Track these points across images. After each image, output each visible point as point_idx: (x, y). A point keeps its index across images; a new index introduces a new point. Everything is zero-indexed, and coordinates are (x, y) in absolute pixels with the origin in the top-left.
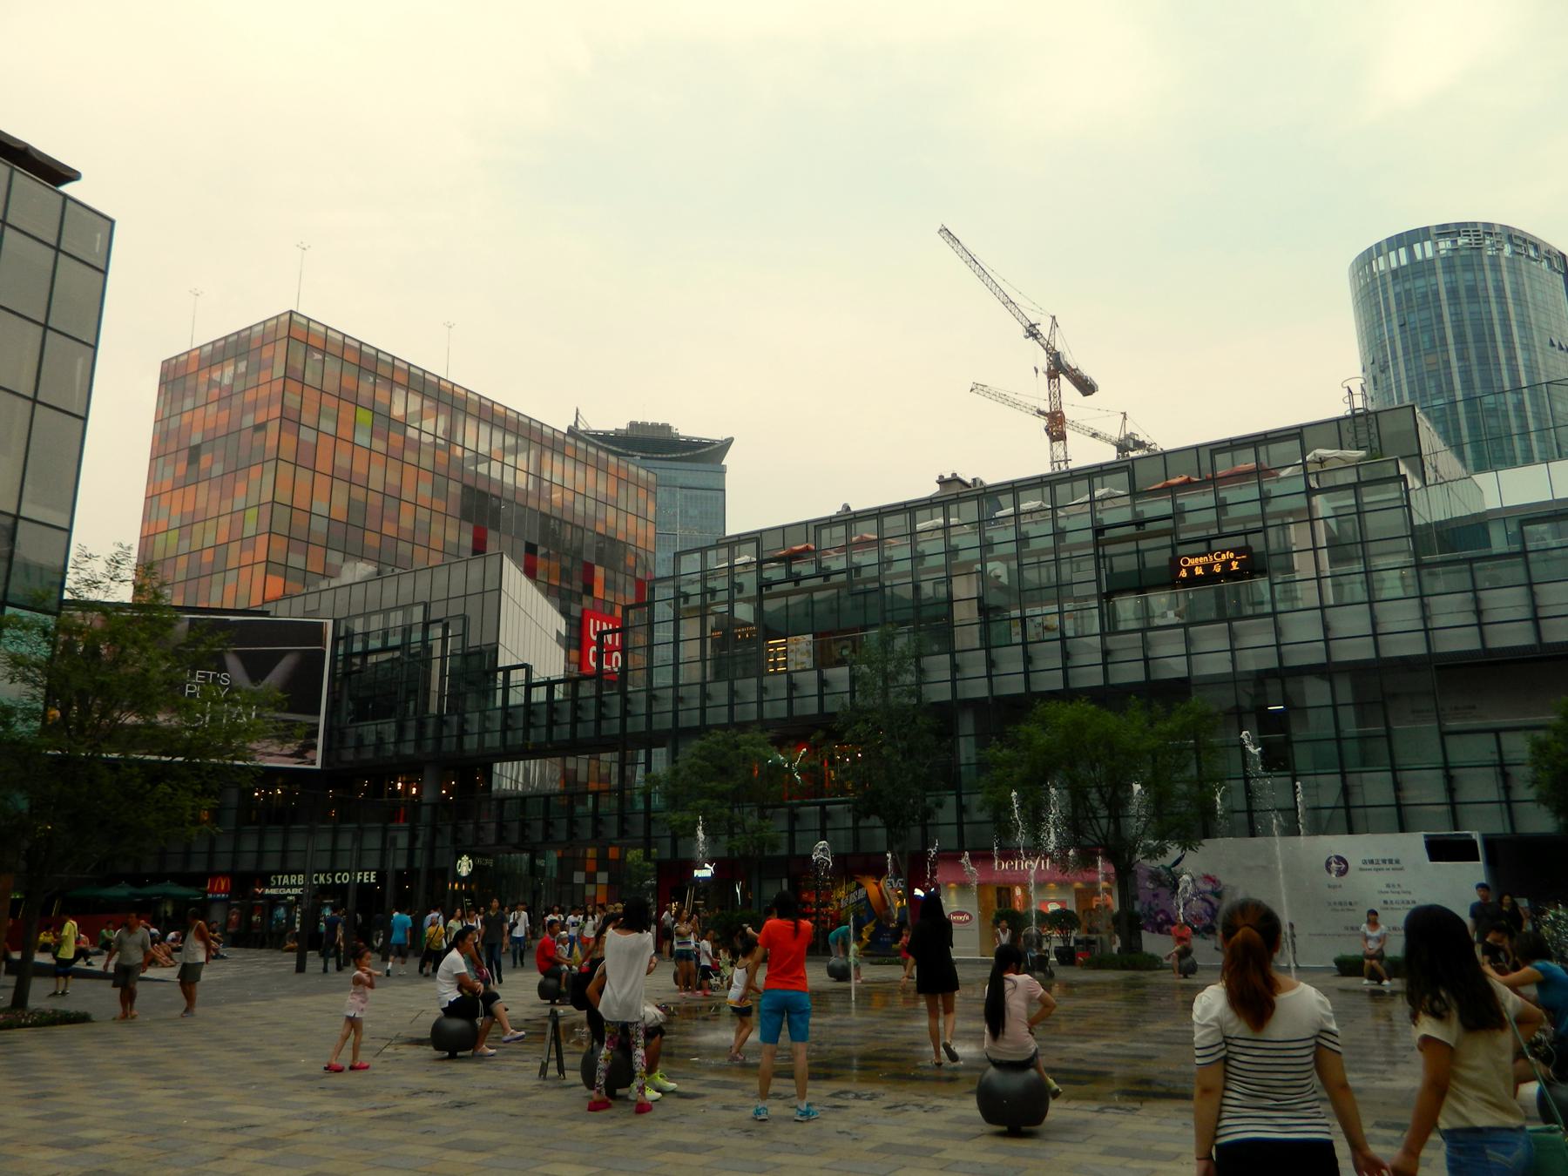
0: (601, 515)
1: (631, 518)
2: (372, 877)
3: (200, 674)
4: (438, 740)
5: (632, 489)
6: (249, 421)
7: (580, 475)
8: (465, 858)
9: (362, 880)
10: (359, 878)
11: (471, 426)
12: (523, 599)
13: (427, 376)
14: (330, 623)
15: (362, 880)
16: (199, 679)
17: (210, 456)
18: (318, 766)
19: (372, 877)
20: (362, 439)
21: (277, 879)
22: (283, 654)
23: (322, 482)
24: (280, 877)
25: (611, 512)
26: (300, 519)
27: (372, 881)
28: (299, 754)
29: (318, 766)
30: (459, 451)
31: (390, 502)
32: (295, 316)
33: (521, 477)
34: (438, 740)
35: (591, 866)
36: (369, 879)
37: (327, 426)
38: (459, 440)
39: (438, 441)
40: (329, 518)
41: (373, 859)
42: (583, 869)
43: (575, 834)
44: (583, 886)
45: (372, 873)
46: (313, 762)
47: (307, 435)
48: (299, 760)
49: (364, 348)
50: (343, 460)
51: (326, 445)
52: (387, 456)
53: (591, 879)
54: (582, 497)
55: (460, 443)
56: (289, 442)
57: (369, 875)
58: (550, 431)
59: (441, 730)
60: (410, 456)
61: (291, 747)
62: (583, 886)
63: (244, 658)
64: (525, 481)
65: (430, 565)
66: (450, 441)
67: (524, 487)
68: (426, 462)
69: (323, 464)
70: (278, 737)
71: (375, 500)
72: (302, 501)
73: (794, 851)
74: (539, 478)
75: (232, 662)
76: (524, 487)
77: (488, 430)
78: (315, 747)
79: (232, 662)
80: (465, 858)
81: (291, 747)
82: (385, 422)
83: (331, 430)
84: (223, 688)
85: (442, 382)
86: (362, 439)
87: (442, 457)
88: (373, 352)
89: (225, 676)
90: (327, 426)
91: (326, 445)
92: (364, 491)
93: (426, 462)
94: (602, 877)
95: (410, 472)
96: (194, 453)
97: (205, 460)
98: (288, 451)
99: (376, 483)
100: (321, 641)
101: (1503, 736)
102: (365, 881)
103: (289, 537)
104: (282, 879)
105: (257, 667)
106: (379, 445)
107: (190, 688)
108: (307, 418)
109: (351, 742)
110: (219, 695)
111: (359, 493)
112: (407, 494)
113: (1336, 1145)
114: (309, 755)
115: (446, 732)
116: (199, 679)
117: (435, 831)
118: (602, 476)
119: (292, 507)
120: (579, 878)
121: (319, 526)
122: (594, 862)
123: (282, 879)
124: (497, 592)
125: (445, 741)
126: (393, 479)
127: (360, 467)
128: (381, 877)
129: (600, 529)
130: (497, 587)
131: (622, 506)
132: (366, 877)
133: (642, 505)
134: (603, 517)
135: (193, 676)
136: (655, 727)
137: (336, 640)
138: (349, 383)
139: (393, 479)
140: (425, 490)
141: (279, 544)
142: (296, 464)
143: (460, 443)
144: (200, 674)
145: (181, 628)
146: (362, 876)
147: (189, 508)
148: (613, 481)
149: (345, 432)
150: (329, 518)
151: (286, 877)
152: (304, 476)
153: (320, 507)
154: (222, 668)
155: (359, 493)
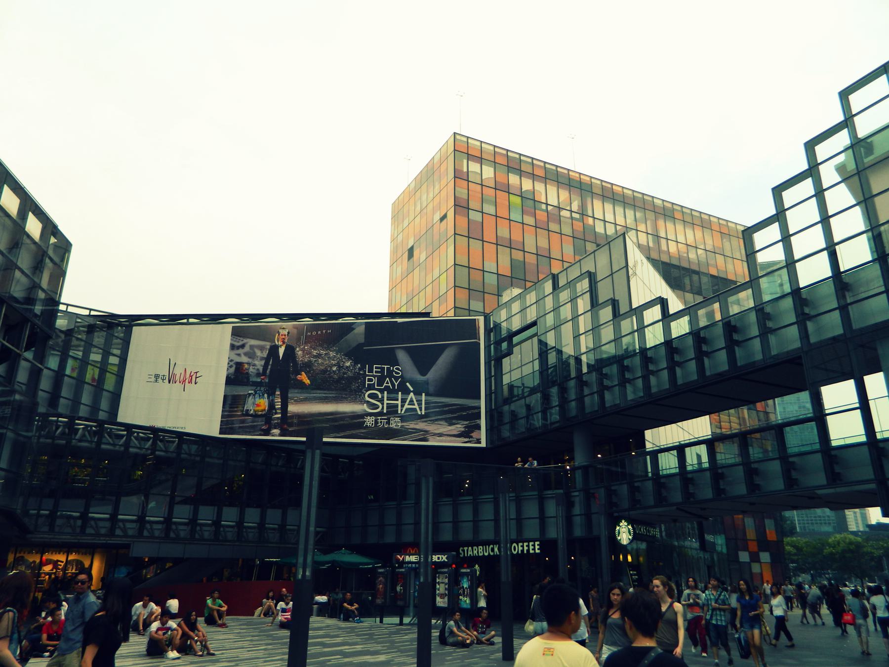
0: (711, 262)
2: (537, 547)
3: (376, 368)
4: (580, 399)
6: (437, 217)
8: (623, 523)
9: (528, 550)
10: (526, 548)
11: (597, 204)
13: (559, 169)
14: (481, 319)
15: (528, 550)
16: (376, 372)
17: (418, 250)
18: (483, 444)
19: (537, 547)
20: (516, 216)
21: (463, 551)
22: (443, 348)
23: (490, 249)
24: (466, 549)
25: (720, 259)
26: (476, 276)
27: (537, 551)
28: (465, 434)
29: (483, 444)
30: (590, 221)
31: (544, 261)
32: (458, 137)
34: (580, 399)
35: (753, 546)
36: (534, 549)
37: (489, 209)
38: (590, 213)
39: (574, 215)
40: (498, 274)
41: (532, 528)
42: (746, 549)
43: (758, 487)
44: (749, 564)
45: (537, 543)
46: (479, 441)
48: (466, 440)
49: (510, 154)
50: (504, 232)
51: (489, 223)
52: (536, 227)
53: (755, 558)
54: (602, 223)
56: (463, 222)
57: (534, 545)
58: (660, 202)
59: (582, 390)
60: (553, 226)
61: (459, 427)
62: (749, 564)
63: (410, 351)
65: (565, 267)
66: (583, 214)
67: (646, 244)
68: (567, 230)
69: (489, 236)
70: (446, 420)
71: (531, 259)
72: (476, 263)
73: (380, 619)
74: (657, 237)
75: (402, 356)
76: (646, 244)
78: (478, 427)
79: (402, 356)
80: (623, 523)
81: (459, 427)
82: (530, 202)
83: (493, 212)
84: (396, 379)
85: (571, 173)
86: (516, 216)
87: (578, 226)
88: (517, 156)
89: (397, 369)
90: (489, 209)
92: (522, 253)
93: (567, 230)
94: (765, 557)
95: (555, 238)
96: (411, 252)
97: (416, 253)
98: (463, 229)
99: (530, 246)
100: (476, 335)
102: (531, 551)
103: (469, 289)
104: (467, 550)
105: (423, 361)
106: (529, 220)
107: (370, 380)
109: (507, 419)
110: (393, 385)
111: (518, 256)
112: (555, 254)
114: (474, 435)
115: (586, 391)
116: (376, 372)
117: (589, 497)
118: (707, 233)
119: (469, 267)
120: (744, 557)
121: (491, 280)
122: (755, 543)
123: (467, 550)
124: (625, 269)
125: (587, 400)
126: (543, 243)
127: (517, 236)
128: (548, 546)
129: (713, 272)
130: (624, 265)
132: (531, 547)
135: (371, 371)
136: (856, 326)
137: (488, 331)
138: (501, 178)
140: (569, 250)
141: (463, 295)
142: (469, 237)
144: (376, 368)
145: (360, 330)
146: (528, 546)
147: (410, 289)
149: (503, 212)
150: (498, 274)
151: (470, 548)
152: (476, 245)
153: (490, 266)
154: (395, 362)
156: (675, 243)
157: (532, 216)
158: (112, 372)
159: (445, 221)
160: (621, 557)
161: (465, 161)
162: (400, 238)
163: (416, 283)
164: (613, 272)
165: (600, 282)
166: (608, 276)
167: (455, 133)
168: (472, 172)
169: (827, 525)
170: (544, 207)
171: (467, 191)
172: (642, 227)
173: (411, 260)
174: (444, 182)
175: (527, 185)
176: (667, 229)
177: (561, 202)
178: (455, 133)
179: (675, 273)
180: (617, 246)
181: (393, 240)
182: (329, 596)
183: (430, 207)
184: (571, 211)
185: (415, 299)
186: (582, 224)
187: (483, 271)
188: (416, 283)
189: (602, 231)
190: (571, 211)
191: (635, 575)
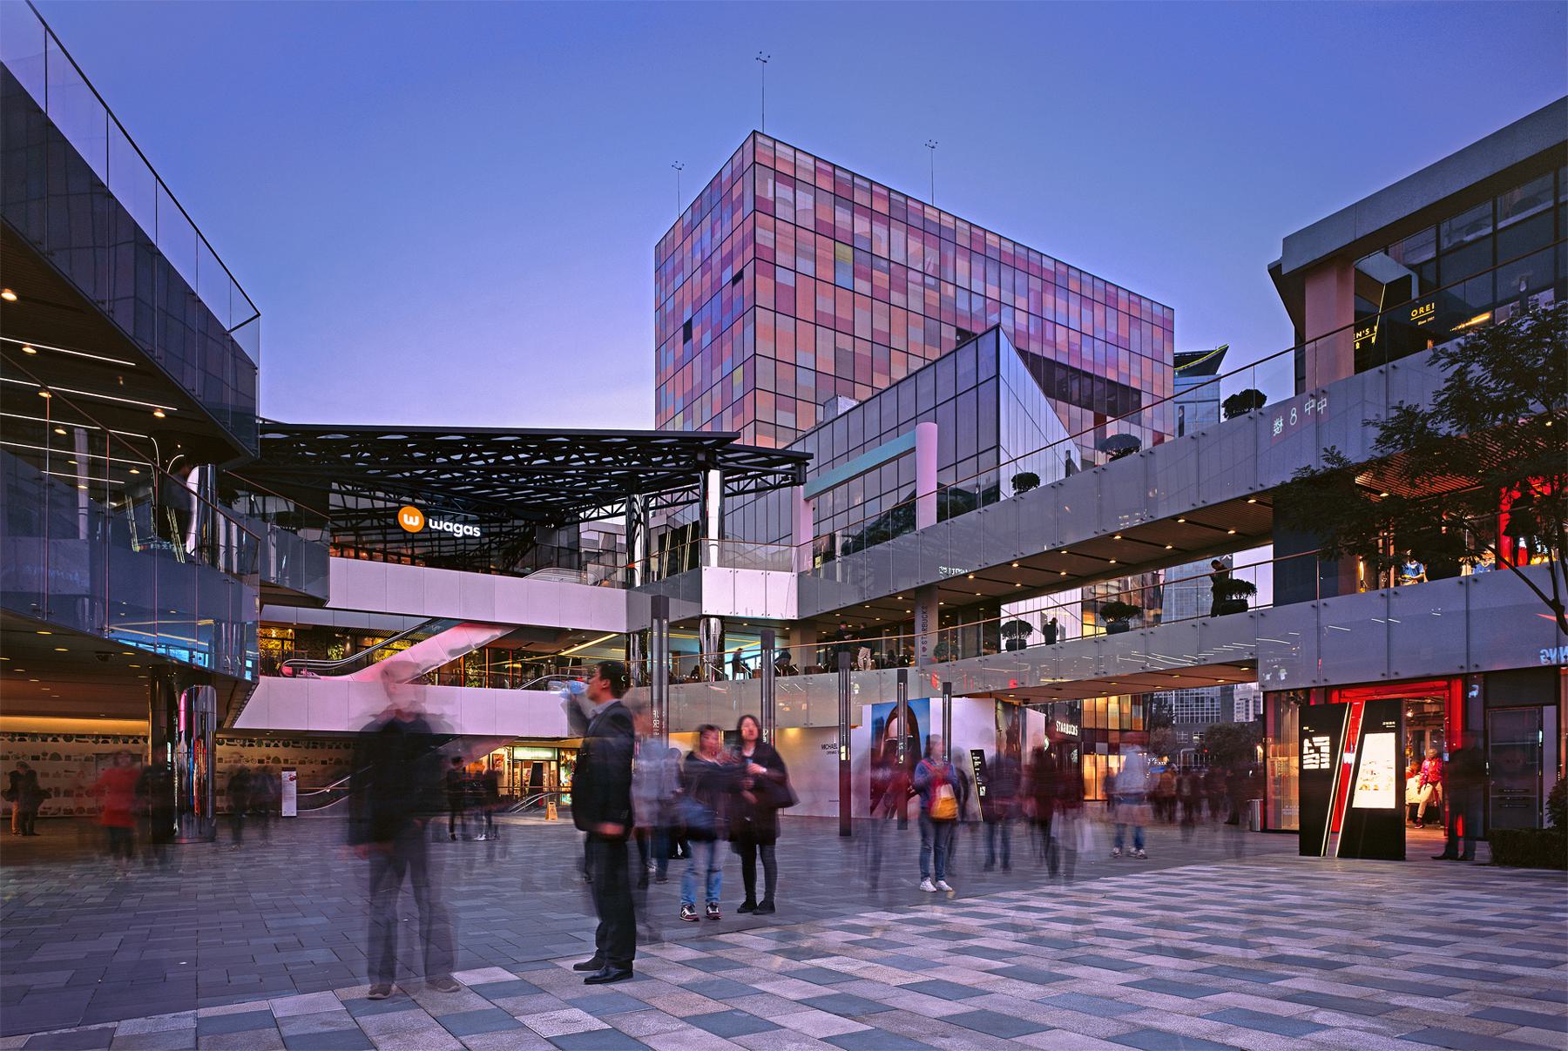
1: (1147, 363)
3: (433, 525)
5: (1146, 327)
6: (728, 276)
7: (1061, 303)
12: (1028, 433)
20: (844, 279)
23: (806, 330)
30: (951, 289)
31: (880, 352)
33: (1021, 318)
37: (805, 266)
47: (785, 278)
50: (826, 305)
51: (805, 287)
54: (966, 294)
55: (951, 279)
60: (897, 298)
64: (1025, 323)
68: (916, 304)
69: (804, 311)
71: (863, 349)
77: (903, 234)
86: (844, 279)
90: (805, 266)
91: (805, 287)
95: (899, 315)
97: (696, 331)
99: (862, 331)
101: (1082, 274)
106: (863, 286)
108: (783, 258)
112: (898, 342)
113: (716, 565)
118: (1111, 313)
124: (994, 380)
127: (845, 314)
131: (1135, 347)
133: (1158, 346)
134: (1052, 338)
139: (880, 324)
140: (917, 335)
143: (951, 279)
144: (433, 525)
147: (688, 388)
148: (1124, 319)
149: (825, 273)
155: (845, 342)
156: (1065, 329)
157: (867, 280)
158: (420, 544)
159: (739, 284)
160: (1487, 767)
161: (771, 182)
162: (670, 306)
163: (697, 379)
164: (979, 382)
165: (903, 241)
166: (971, 389)
167: (754, 132)
168: (779, 198)
169: (648, 942)
170: (884, 264)
171: (773, 234)
172: (1021, 303)
173: (689, 342)
174: (738, 217)
175: (862, 226)
176: (1056, 305)
177: (911, 254)
178: (754, 132)
179: (1059, 374)
180: (987, 343)
181: (659, 308)
182: (768, 771)
183: (717, 258)
184: (924, 274)
185: (697, 404)
186: (938, 294)
187: (796, 365)
188: (697, 379)
189: (966, 308)
190: (924, 274)
191: (978, 760)
